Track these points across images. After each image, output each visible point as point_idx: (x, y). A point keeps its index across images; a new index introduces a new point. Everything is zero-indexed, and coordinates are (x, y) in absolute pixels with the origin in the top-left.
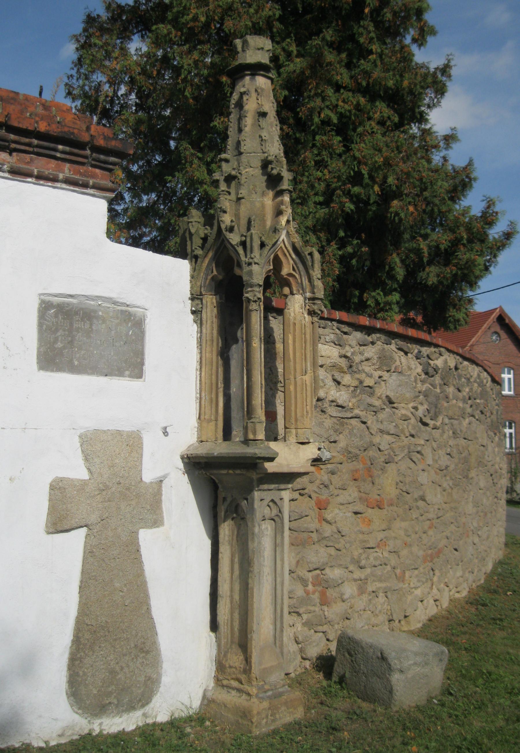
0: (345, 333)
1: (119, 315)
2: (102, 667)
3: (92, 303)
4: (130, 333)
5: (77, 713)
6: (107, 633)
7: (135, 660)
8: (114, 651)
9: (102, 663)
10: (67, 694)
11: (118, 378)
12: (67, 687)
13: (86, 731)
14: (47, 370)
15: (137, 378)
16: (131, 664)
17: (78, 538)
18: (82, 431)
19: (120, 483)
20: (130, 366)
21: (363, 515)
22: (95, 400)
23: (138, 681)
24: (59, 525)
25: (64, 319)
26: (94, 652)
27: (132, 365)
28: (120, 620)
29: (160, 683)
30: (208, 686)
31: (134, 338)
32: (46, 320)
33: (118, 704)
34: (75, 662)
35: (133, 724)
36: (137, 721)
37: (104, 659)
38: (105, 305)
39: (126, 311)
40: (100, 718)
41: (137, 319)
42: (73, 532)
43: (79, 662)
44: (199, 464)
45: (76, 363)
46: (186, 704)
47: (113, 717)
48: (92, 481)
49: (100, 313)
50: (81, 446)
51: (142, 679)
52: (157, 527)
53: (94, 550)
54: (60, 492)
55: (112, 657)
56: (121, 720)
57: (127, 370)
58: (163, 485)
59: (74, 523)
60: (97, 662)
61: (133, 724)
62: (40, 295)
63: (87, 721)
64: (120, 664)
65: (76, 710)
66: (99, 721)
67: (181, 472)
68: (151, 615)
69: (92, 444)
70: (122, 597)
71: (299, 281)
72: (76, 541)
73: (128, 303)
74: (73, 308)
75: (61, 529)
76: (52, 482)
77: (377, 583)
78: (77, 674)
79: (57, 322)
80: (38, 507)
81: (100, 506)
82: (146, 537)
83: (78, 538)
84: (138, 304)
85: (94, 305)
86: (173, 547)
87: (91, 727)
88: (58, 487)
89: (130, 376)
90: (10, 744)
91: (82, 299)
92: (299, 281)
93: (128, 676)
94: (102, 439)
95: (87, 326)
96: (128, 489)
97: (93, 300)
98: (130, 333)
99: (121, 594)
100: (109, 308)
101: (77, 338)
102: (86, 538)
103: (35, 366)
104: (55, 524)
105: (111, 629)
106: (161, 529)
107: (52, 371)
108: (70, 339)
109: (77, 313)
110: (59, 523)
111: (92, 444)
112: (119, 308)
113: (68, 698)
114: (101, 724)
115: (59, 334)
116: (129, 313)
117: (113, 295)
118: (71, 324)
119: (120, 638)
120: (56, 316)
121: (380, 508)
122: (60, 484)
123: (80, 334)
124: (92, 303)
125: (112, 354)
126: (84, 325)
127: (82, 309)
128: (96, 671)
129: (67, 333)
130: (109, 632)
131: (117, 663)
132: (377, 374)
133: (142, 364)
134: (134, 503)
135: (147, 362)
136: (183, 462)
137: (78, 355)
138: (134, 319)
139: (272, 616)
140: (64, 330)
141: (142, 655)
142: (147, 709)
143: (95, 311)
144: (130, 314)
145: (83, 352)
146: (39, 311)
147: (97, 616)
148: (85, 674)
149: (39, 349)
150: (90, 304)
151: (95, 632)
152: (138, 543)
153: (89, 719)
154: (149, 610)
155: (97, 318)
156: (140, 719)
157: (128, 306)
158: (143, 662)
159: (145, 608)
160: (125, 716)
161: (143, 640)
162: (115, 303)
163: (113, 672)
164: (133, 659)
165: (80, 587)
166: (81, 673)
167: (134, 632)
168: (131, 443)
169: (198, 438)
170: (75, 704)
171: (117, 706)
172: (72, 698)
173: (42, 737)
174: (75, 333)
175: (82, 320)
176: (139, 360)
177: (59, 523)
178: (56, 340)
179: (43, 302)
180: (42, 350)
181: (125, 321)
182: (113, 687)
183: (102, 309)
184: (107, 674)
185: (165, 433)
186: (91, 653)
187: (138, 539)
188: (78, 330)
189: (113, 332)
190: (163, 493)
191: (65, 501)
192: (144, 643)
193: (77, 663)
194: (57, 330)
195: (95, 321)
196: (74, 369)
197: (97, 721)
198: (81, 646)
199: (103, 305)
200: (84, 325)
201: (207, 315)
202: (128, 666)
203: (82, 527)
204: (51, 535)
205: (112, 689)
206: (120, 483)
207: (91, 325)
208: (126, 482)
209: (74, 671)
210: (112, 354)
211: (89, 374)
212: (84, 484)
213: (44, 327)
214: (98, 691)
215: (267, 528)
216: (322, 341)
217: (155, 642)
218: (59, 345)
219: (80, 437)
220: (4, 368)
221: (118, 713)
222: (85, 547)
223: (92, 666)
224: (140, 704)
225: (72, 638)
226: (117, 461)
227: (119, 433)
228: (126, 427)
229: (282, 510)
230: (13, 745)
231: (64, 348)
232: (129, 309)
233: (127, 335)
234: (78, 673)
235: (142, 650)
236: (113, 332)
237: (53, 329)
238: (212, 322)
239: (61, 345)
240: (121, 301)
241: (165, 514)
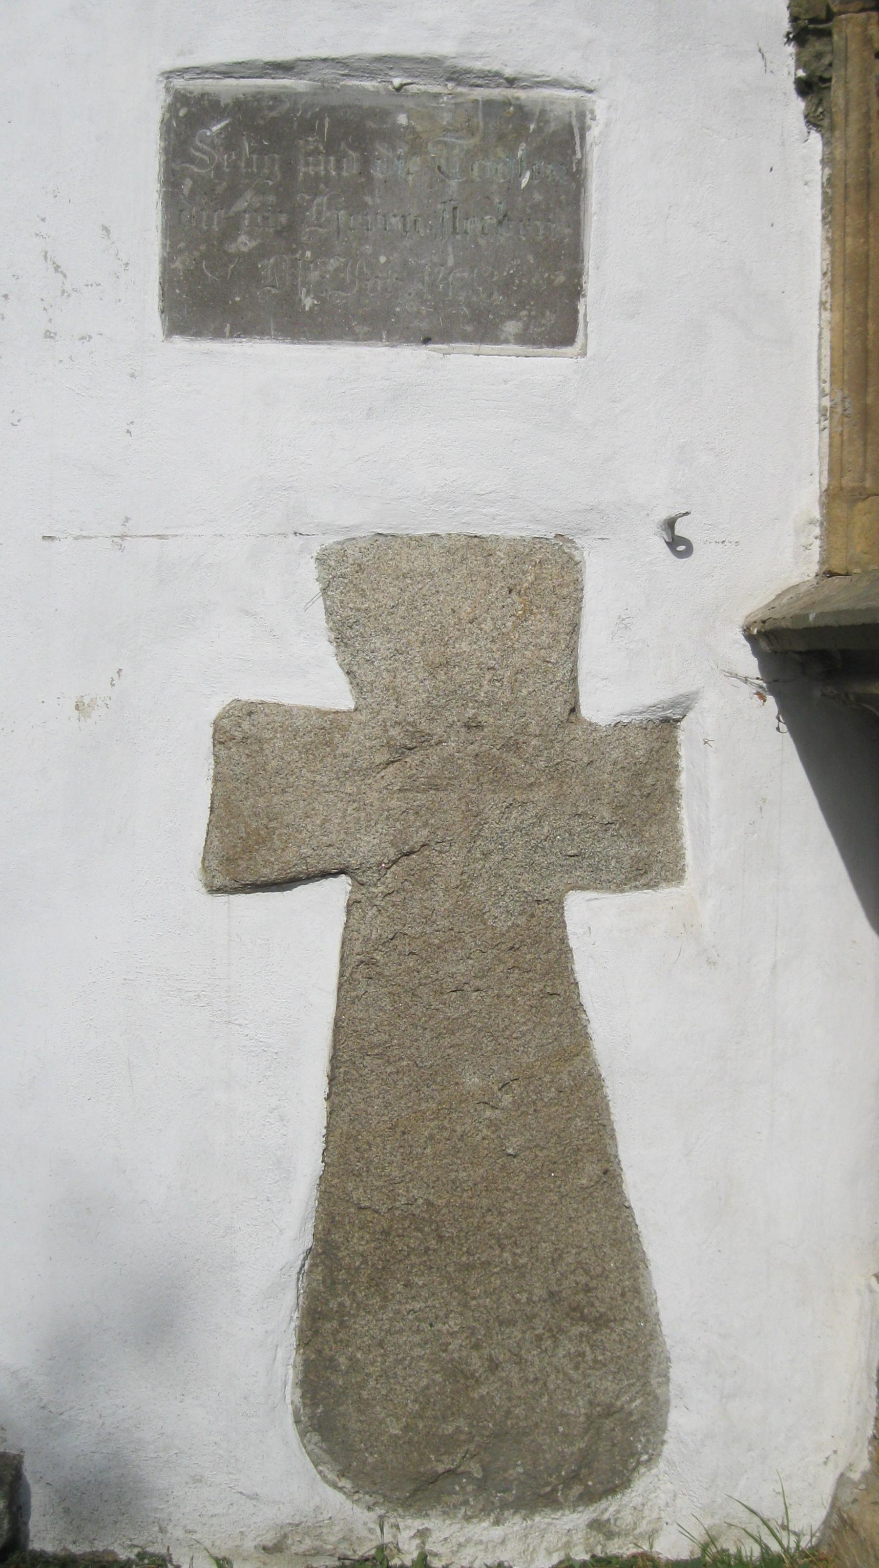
1: (479, 120)
2: (418, 1351)
3: (369, 84)
4: (524, 182)
5: (335, 1486)
6: (433, 1244)
7: (548, 1343)
8: (466, 1305)
9: (417, 1339)
10: (297, 1422)
11: (475, 347)
12: (298, 1400)
13: (367, 1549)
14: (198, 334)
15: (554, 343)
16: (532, 1355)
17: (319, 914)
18: (330, 540)
19: (480, 726)
20: (522, 304)
22: (414, 431)
23: (562, 1415)
24: (243, 864)
25: (261, 151)
26: (385, 1299)
27: (532, 291)
28: (485, 1202)
29: (664, 1429)
30: (850, 1467)
31: (538, 197)
32: (192, 160)
33: (485, 1478)
34: (323, 1320)
35: (549, 1553)
36: (568, 1545)
37: (425, 1326)
38: (419, 86)
39: (507, 103)
40: (422, 1513)
41: (553, 126)
42: (301, 892)
43: (335, 1324)
44: (822, 656)
45: (308, 302)
46: (766, 1514)
47: (468, 1519)
48: (362, 717)
49: (402, 119)
50: (324, 590)
51: (579, 1408)
52: (647, 886)
53: (378, 956)
54: (253, 753)
55: (453, 1324)
56: (498, 1532)
57: (511, 317)
58: (682, 736)
59: (291, 858)
60: (401, 1331)
61: (549, 1553)
62: (169, 75)
63: (373, 1516)
64: (485, 1352)
65: (332, 1476)
66: (418, 1524)
67: (747, 691)
68: (621, 1193)
69: (365, 586)
70: (493, 1125)
73: (508, 72)
74: (294, 110)
75: (250, 878)
76: (220, 717)
78: (332, 1364)
79: (234, 166)
80: (175, 799)
81: (394, 803)
82: (593, 920)
83: (319, 914)
84: (554, 71)
85: (377, 93)
86: (712, 963)
87: (388, 1538)
88: (239, 735)
89: (524, 339)
90: (100, 1546)
91: (329, 73)
93: (521, 1393)
94: (405, 567)
95: (351, 169)
96: (512, 746)
97: (371, 74)
98: (524, 182)
99: (488, 1113)
100: (437, 96)
101: (311, 214)
102: (349, 912)
103: (155, 322)
104: (229, 861)
105: (449, 1231)
106: (665, 895)
107: (218, 334)
108: (283, 219)
109: (308, 127)
110: (248, 859)
111: (365, 586)
112: (480, 94)
113: (302, 1434)
114: (422, 1534)
115: (241, 204)
116: (520, 107)
117: (445, 47)
118: (289, 169)
119: (486, 1264)
120: (230, 141)
122: (246, 725)
123: (323, 200)
124: (369, 84)
125: (451, 262)
126: (339, 168)
127: (331, 110)
128: (399, 1362)
129: (272, 199)
130: (440, 1238)
131: (477, 1346)
133: (574, 290)
134: (539, 796)
135: (592, 284)
136: (756, 652)
137: (314, 276)
138: (539, 130)
140: (261, 191)
141: (575, 1330)
142: (609, 1508)
143: (383, 114)
144: (522, 113)
145: (333, 263)
147: (392, 1182)
148: (354, 1365)
149: (166, 262)
150: (364, 91)
151: (386, 1233)
152: (564, 940)
153: (380, 1511)
154: (610, 1175)
155: (391, 136)
156: (578, 1537)
157: (511, 82)
158: (583, 1354)
159: (592, 1169)
160: (515, 1524)
161: (583, 1279)
162: (457, 76)
163: (457, 1373)
164: (539, 1338)
165: (332, 1079)
166: (342, 1360)
167: (545, 1249)
168: (538, 583)
169: (822, 562)
170: (326, 1457)
171: (482, 1486)
172: (316, 1438)
173: (208, 1544)
174: (302, 197)
175: (331, 147)
176: (561, 279)
177: (248, 859)
178: (231, 229)
179: (180, 99)
180: (178, 264)
181: (501, 137)
182: (462, 1422)
183: (410, 104)
184: (438, 1377)
185: (679, 546)
186: (376, 1301)
187: (563, 925)
188: (314, 185)
189: (454, 183)
190: (683, 763)
191: (263, 783)
192: (587, 1289)
193: (329, 1326)
194: (234, 192)
195: (381, 149)
196: (297, 325)
197: (409, 1522)
198: (342, 1275)
199: (413, 89)
200: (339, 168)
201: (847, 92)
202: (520, 1361)
203: (325, 874)
204: (223, 898)
205: (458, 1430)
206: (480, 726)
207: (366, 162)
208: (506, 722)
209: (319, 1352)
210: (451, 262)
211: (356, 338)
212: (328, 727)
213: (188, 184)
214: (406, 1428)
217: (637, 1291)
218: (244, 243)
219: (321, 560)
220: (48, 335)
221: (485, 1510)
222: (345, 942)
223: (381, 1344)
224: (577, 1489)
225: (308, 1241)
226: (464, 646)
227: (478, 545)
228: (511, 525)
230: (112, 1552)
231: (262, 251)
232: (522, 94)
234: (332, 1359)
235: (577, 1313)
237: (220, 190)
238: (867, 115)
239: (252, 244)
240: (478, 65)
241: (688, 841)
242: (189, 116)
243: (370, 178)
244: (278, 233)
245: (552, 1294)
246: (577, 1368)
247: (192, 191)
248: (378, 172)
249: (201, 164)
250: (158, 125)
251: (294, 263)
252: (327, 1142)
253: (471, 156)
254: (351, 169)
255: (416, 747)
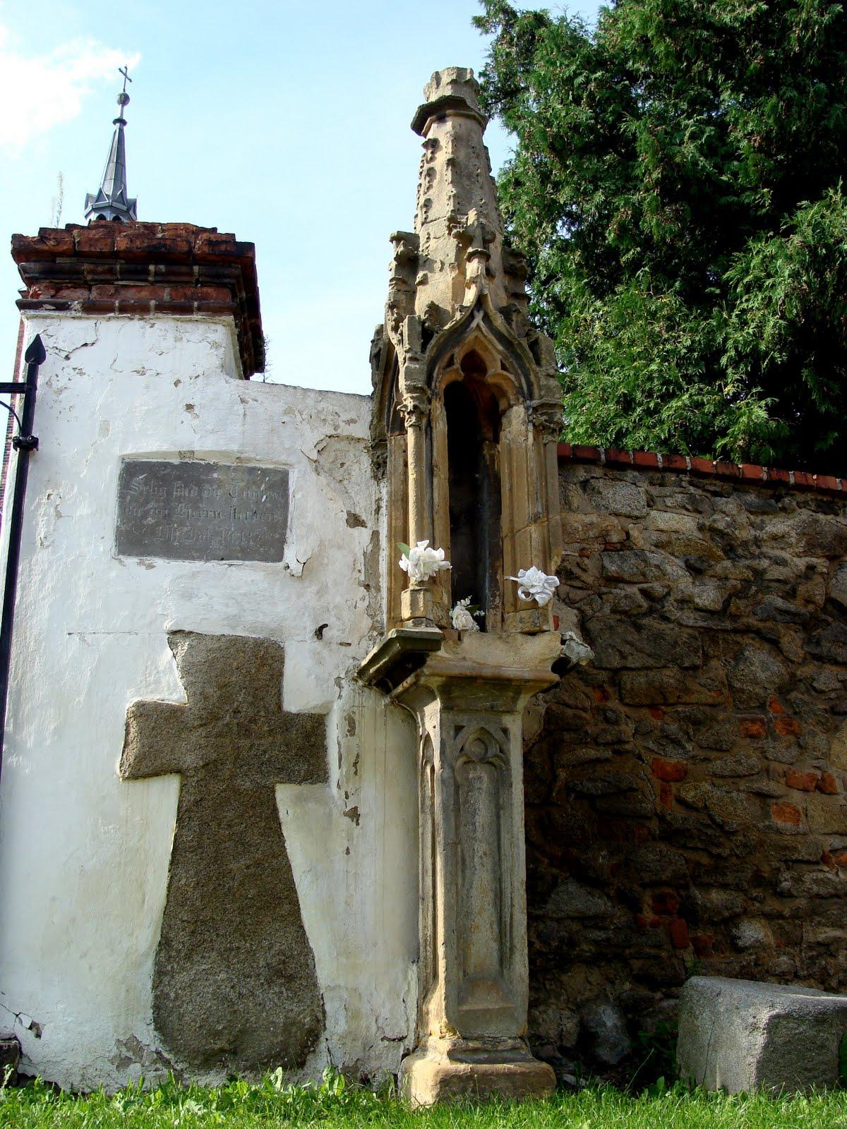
0: (715, 494)
8: (229, 967)
21: (781, 801)
27: (264, 540)
31: (268, 505)
68: (300, 920)
71: (516, 383)
72: (164, 797)
77: (827, 930)
92: (516, 383)
95: (194, 493)
110: (143, 769)
115: (150, 506)
118: (169, 493)
119: (238, 948)
121: (822, 791)
126: (189, 493)
129: (162, 504)
132: (801, 563)
139: (495, 926)
146: (121, 477)
158: (282, 993)
161: (283, 958)
164: (262, 984)
166: (172, 995)
176: (277, 536)
177: (143, 769)
188: (179, 500)
189: (235, 500)
192: (284, 962)
193: (166, 979)
194: (147, 502)
200: (189, 493)
202: (253, 994)
215: (480, 778)
216: (659, 505)
218: (150, 520)
229: (504, 747)
231: (157, 524)
233: (258, 502)
234: (168, 994)
236: (235, 500)
242: (132, 470)
243: (201, 497)
244: (164, 517)
245: (268, 964)
246: (279, 999)
247: (130, 502)
248: (205, 495)
249: (135, 490)
250: (416, 109)
251: (170, 529)
252: (169, 891)
253: (242, 490)
254: (194, 493)
255: (139, 840)
